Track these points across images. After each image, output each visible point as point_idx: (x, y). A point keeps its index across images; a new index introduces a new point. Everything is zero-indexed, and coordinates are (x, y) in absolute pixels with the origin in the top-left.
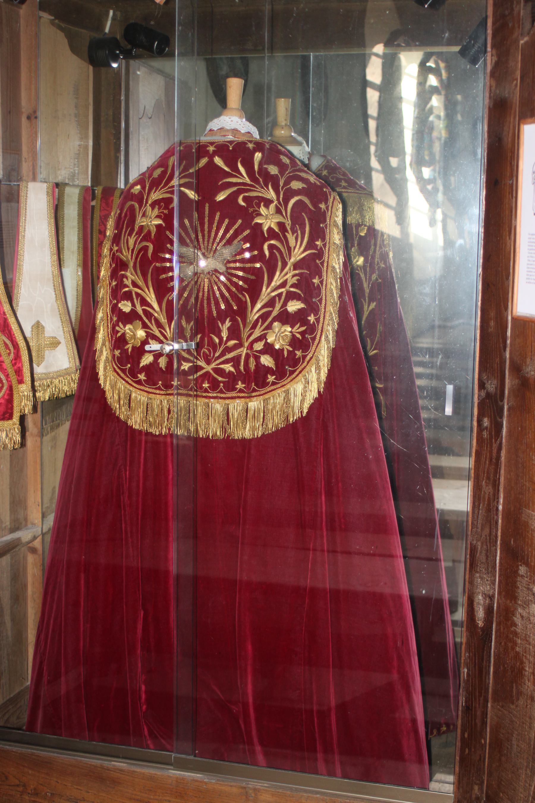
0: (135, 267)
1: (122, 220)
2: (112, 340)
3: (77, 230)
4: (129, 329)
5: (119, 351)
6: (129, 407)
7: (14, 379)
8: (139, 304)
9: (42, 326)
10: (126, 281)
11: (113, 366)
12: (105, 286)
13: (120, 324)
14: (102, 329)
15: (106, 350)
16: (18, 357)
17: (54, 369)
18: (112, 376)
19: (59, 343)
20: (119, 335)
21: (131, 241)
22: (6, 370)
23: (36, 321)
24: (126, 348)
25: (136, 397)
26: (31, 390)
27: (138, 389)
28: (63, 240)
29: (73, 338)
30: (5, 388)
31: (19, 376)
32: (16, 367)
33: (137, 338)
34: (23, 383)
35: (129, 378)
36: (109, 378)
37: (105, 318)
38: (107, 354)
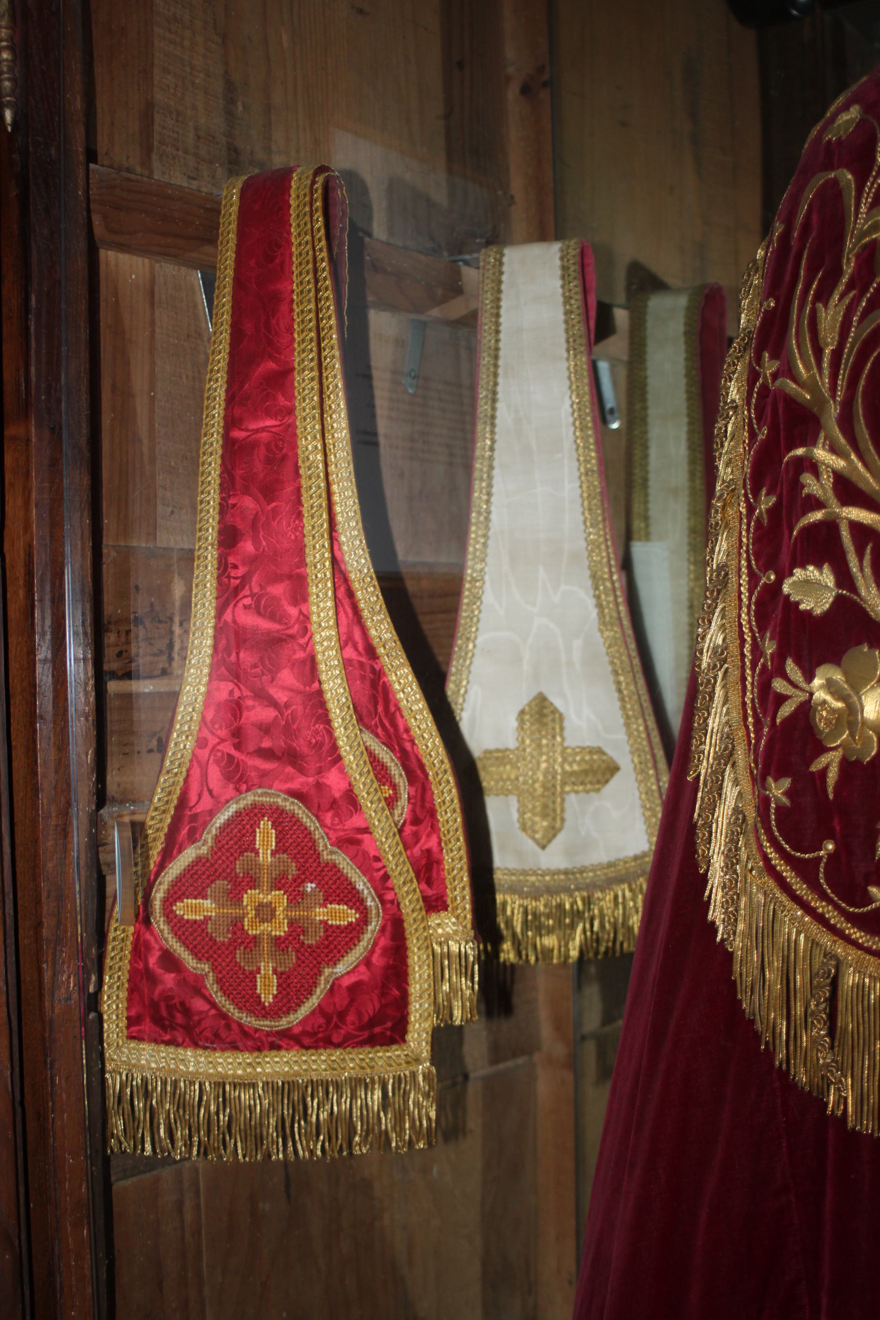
0: (846, 422)
1: (794, 251)
2: (758, 739)
3: (686, 420)
4: (830, 686)
5: (786, 783)
6: (831, 1033)
7: (408, 894)
8: (868, 570)
9: (555, 711)
10: (811, 485)
11: (760, 847)
12: (735, 524)
13: (790, 666)
14: (719, 692)
15: (736, 782)
16: (423, 813)
17: (599, 856)
18: (759, 890)
19: (613, 769)
20: (786, 710)
21: (830, 317)
22: (378, 859)
23: (534, 693)
24: (813, 769)
25: (860, 987)
26: (472, 933)
27: (868, 951)
28: (646, 456)
29: (660, 753)
30: (374, 926)
31: (429, 883)
32: (417, 851)
33: (864, 722)
34: (445, 908)
35: (830, 901)
36: (743, 900)
37: (734, 648)
38: (740, 795)
